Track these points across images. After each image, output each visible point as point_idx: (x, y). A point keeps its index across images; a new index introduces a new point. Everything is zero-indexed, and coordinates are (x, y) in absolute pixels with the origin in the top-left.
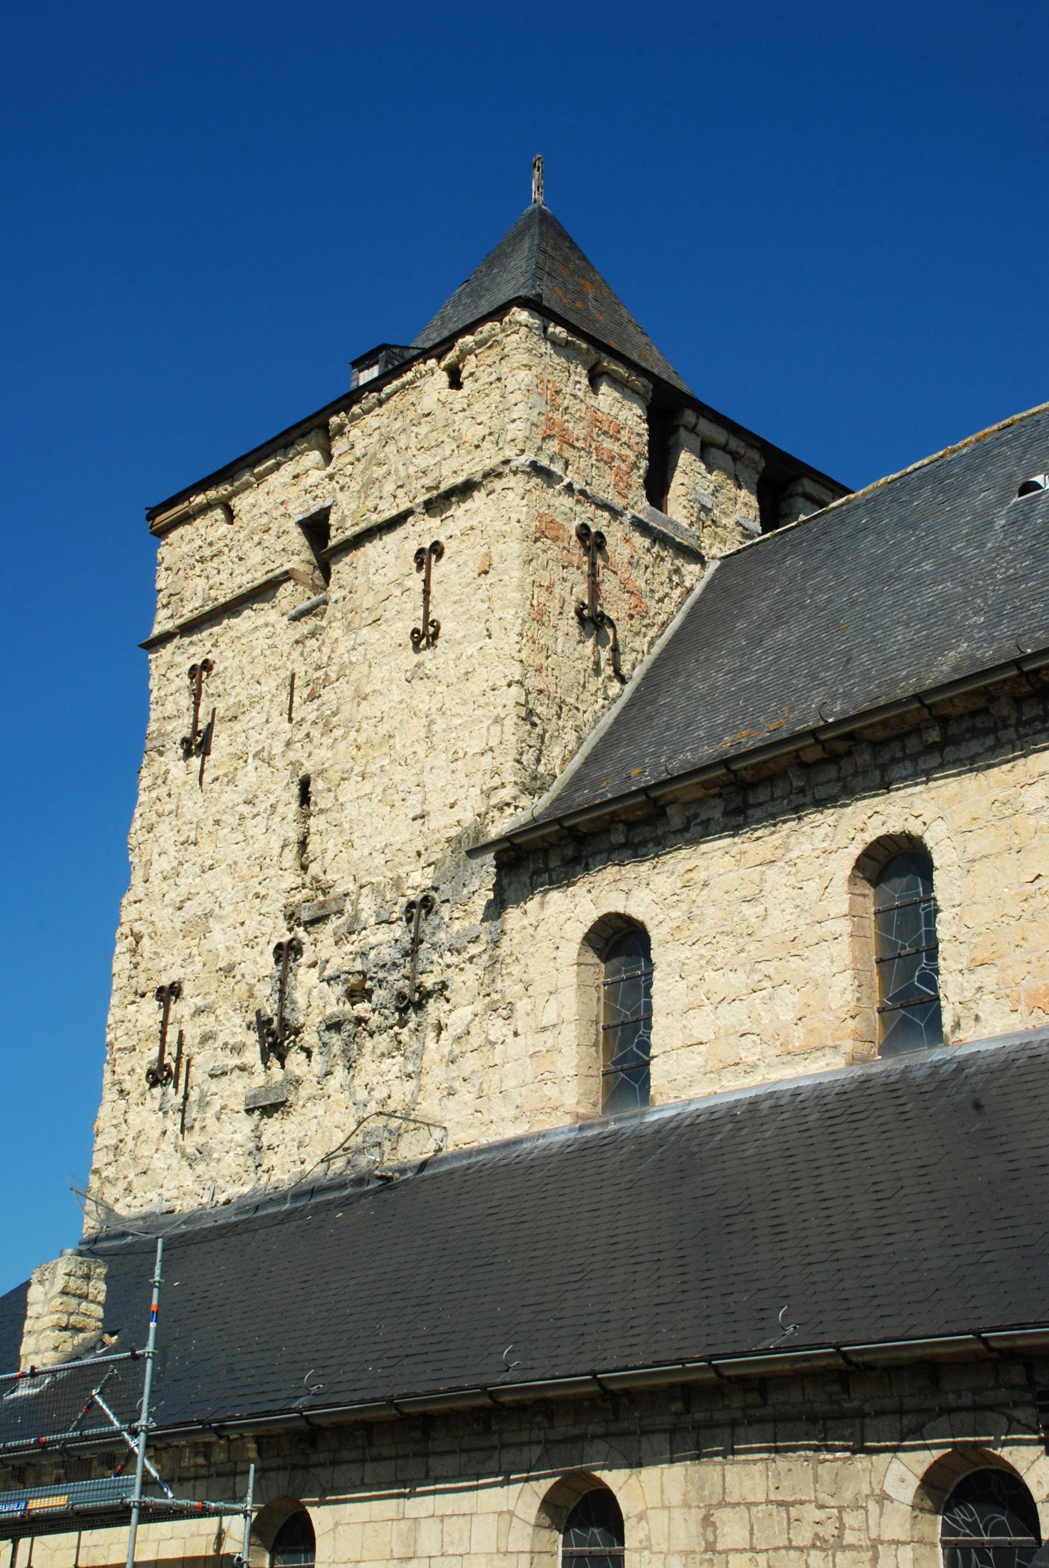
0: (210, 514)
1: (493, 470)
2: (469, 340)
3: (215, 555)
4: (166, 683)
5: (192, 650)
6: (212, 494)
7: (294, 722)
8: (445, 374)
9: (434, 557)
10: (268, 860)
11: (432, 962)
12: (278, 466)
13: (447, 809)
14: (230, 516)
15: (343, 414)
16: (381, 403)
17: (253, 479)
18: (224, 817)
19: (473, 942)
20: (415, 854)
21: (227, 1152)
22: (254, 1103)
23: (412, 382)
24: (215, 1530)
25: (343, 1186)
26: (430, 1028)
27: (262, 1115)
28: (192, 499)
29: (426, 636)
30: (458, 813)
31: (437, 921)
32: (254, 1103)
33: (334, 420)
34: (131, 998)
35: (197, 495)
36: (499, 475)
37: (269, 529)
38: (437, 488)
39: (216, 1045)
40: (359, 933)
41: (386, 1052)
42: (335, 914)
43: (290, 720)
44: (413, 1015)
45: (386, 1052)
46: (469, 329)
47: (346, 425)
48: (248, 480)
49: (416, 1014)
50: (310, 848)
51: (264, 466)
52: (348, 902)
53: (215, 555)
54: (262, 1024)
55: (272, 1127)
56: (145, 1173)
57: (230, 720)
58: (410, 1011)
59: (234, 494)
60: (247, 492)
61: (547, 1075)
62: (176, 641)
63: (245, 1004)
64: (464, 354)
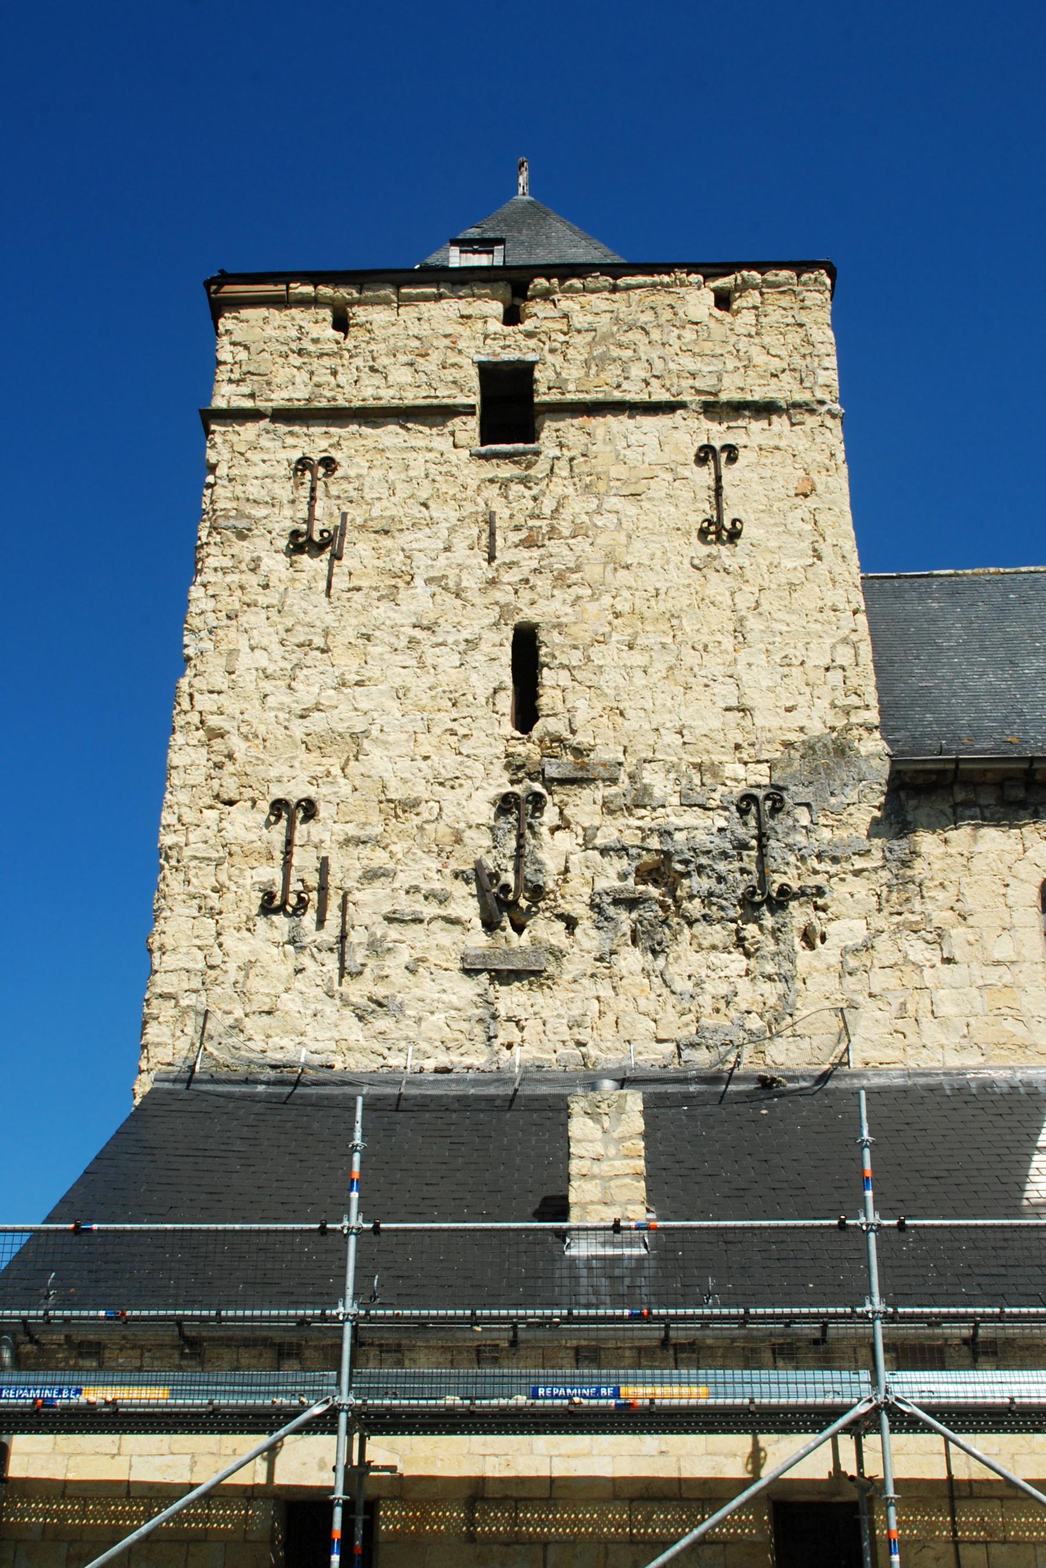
0: (313, 310)
1: (807, 404)
2: (755, 275)
3: (327, 354)
4: (243, 462)
5: (290, 441)
6: (326, 291)
7: (497, 562)
8: (712, 294)
10: (470, 697)
11: (788, 864)
12: (439, 298)
13: (782, 711)
14: (341, 323)
15: (555, 281)
16: (614, 289)
17: (394, 298)
18: (377, 633)
19: (860, 855)
21: (432, 1013)
22: (483, 963)
23: (668, 286)
24: (749, 1449)
25: (685, 1081)
26: (795, 933)
27: (492, 980)
28: (292, 285)
29: (720, 531)
30: (797, 719)
31: (790, 822)
33: (541, 282)
34: (209, 801)
35: (304, 284)
36: (812, 412)
37: (427, 355)
38: (716, 395)
40: (654, 809)
41: (721, 945)
42: (604, 780)
43: (491, 558)
44: (768, 914)
45: (721, 945)
46: (762, 267)
47: (556, 293)
48: (387, 296)
49: (773, 915)
51: (419, 291)
53: (327, 354)
54: (483, 879)
55: (511, 999)
56: (269, 1013)
57: (376, 532)
58: (765, 908)
59: (359, 303)
60: (381, 308)
61: (1004, 1011)
62: (265, 423)
63: (449, 849)
64: (745, 286)
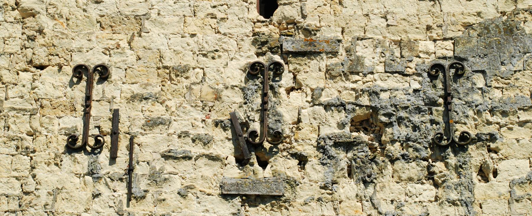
9: (97, 77)
11: (467, 117)
20: (425, 27)
22: (237, 190)
26: (473, 169)
31: (469, 85)
32: (237, 190)
34: (24, 66)
39: (171, 131)
41: (416, 178)
42: (327, 53)
44: (452, 155)
50: (147, 97)
52: (341, 47)
54: (236, 127)
58: (450, 149)
63: (211, 104)
